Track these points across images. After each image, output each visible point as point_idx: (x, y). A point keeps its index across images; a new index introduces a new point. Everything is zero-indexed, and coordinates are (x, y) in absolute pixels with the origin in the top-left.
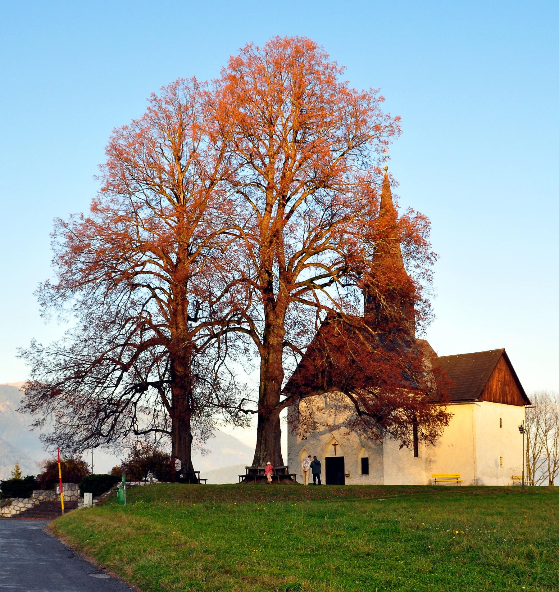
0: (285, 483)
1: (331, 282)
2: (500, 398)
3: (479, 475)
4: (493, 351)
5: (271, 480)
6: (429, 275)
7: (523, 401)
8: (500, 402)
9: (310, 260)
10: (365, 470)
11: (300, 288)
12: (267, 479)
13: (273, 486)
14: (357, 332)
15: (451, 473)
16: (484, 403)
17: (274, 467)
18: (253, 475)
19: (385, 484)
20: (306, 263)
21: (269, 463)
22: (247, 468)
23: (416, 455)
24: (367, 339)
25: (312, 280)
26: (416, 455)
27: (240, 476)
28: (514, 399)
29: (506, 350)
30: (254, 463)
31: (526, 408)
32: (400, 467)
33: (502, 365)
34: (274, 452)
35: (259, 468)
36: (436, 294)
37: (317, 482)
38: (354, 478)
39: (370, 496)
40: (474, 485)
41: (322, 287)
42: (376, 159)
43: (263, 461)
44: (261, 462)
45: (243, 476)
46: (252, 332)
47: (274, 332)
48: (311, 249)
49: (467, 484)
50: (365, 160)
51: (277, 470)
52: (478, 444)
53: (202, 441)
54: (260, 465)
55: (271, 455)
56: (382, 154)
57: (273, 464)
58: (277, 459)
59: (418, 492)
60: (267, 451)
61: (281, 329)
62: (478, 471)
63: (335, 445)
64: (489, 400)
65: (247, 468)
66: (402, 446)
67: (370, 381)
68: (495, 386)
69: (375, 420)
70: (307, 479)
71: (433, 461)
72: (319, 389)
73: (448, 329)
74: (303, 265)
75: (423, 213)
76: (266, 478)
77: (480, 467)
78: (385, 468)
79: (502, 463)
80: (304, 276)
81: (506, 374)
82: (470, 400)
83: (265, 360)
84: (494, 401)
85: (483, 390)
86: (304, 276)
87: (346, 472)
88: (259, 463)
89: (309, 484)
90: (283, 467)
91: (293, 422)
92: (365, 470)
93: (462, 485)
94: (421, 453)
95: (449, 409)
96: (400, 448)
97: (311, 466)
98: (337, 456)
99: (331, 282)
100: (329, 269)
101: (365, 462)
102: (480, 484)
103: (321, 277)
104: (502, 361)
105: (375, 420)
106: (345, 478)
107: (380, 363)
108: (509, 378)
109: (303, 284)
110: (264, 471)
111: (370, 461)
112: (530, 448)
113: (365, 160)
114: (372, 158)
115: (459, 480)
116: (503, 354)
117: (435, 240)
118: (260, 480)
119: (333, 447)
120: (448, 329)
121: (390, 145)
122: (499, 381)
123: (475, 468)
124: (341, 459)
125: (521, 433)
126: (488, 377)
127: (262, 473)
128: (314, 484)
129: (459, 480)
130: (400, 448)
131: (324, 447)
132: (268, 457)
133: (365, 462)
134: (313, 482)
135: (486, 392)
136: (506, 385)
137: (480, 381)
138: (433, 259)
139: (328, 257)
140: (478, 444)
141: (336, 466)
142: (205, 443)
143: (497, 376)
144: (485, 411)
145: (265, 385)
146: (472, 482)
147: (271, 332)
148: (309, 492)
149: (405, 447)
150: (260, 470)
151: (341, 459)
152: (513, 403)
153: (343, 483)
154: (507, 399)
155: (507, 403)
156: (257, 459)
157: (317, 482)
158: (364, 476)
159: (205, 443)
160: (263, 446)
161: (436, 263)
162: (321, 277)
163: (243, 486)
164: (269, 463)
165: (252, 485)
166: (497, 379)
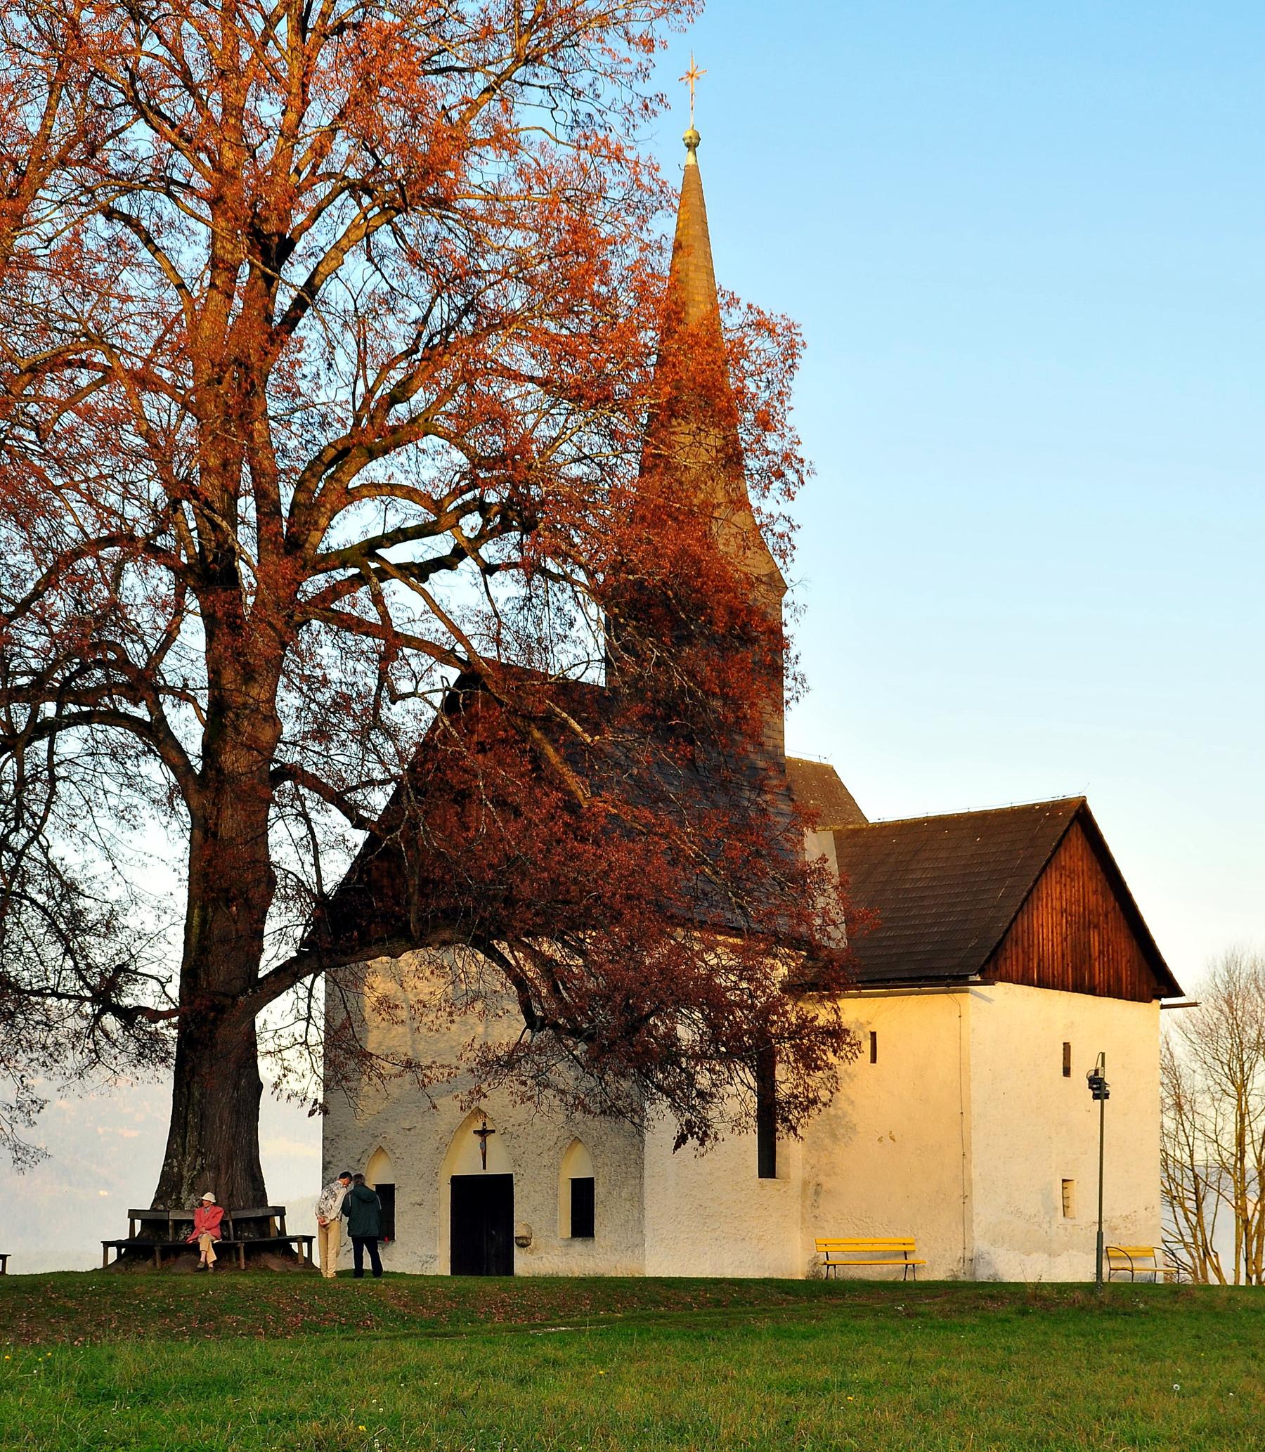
0: (266, 1270)
1: (458, 554)
2: (1065, 971)
3: (980, 1244)
4: (1044, 807)
5: (212, 1257)
6: (782, 536)
7: (1154, 984)
8: (1063, 987)
9: (377, 471)
10: (583, 1226)
11: (340, 575)
12: (199, 1254)
13: (225, 1279)
14: (537, 734)
15: (888, 1239)
16: (1001, 988)
17: (229, 1209)
18: (154, 1241)
19: (650, 1272)
20: (354, 483)
21: (209, 1197)
22: (134, 1214)
23: (768, 1167)
24: (570, 760)
25: (370, 548)
26: (768, 1167)
27: (107, 1245)
28: (1119, 979)
29: (1090, 803)
30: (160, 1196)
31: (1163, 1007)
32: (701, 1213)
33: (1076, 854)
34: (231, 1158)
35: (174, 1215)
36: (799, 603)
37: (367, 1264)
38: (545, 1253)
39: (530, 1316)
40: (962, 1278)
41: (417, 573)
42: (619, 106)
43: (192, 1189)
44: (184, 1195)
45: (118, 1244)
46: (157, 736)
47: (238, 733)
48: (373, 435)
49: (939, 1274)
50: (584, 107)
51: (237, 1222)
52: (985, 1132)
53: (20, 1116)
54: (179, 1205)
55: (218, 1168)
56: (639, 86)
57: (226, 1201)
58: (242, 1182)
59: (718, 1303)
60: (204, 1155)
61: (265, 718)
62: (977, 1231)
63: (483, 1133)
64: (1025, 980)
65: (134, 1214)
66: (681, 1140)
67: (564, 913)
68: (1048, 926)
69: (616, 1043)
70: (332, 1254)
71: (829, 1192)
72: (401, 937)
73: (885, 720)
74: (348, 491)
75: (772, 308)
76: (195, 1249)
77: (985, 1212)
78: (649, 1213)
79: (1071, 1203)
80: (349, 527)
81: (1091, 886)
82: (948, 977)
83: (206, 831)
84: (1042, 984)
85: (1001, 943)
86: (349, 527)
87: (518, 1231)
88: (179, 1198)
89: (340, 1274)
90: (260, 1213)
91: (344, 1052)
92: (583, 1226)
93: (922, 1277)
94: (787, 1164)
95: (856, 1011)
96: (677, 1146)
97: (345, 1209)
98: (491, 1171)
99: (458, 554)
100: (437, 506)
101: (583, 1192)
102: (983, 1275)
103: (401, 535)
104: (1077, 842)
105: (616, 1043)
106: (516, 1250)
107: (640, 846)
108: (1098, 901)
109: (342, 558)
110: (190, 1223)
111: (599, 1191)
112: (1249, 1149)
113: (584, 107)
114: (605, 100)
115: (911, 1259)
116: (1078, 817)
117: (814, 411)
118: (177, 1255)
119: (478, 1139)
120: (885, 720)
121: (658, 54)
122: (1064, 911)
123: (965, 1220)
124: (503, 1185)
125: (1096, 1097)
126: (1033, 899)
127: (185, 1231)
128: (359, 1271)
129: (911, 1259)
130: (677, 1146)
131: (446, 1139)
132: (209, 1175)
133: (583, 1192)
134: (352, 1266)
135: (1013, 952)
136: (1091, 925)
137: (990, 913)
138: (791, 476)
139: (432, 464)
140: (985, 1132)
141: (483, 1213)
142: (32, 1124)
143: (1056, 894)
144: (1013, 1024)
145: (204, 921)
146: (955, 1266)
147: (230, 731)
148: (300, 1302)
149: (692, 1142)
150: (179, 1224)
151: (503, 1185)
152: (1113, 990)
153: (509, 1269)
154: (1092, 976)
155: (1092, 991)
156: (169, 1186)
157: (367, 1264)
158: (578, 1245)
159: (32, 1124)
160: (192, 1137)
161: (800, 493)
162: (401, 535)
163: (118, 1279)
164: (209, 1197)
165: (144, 1275)
166: (1057, 904)
